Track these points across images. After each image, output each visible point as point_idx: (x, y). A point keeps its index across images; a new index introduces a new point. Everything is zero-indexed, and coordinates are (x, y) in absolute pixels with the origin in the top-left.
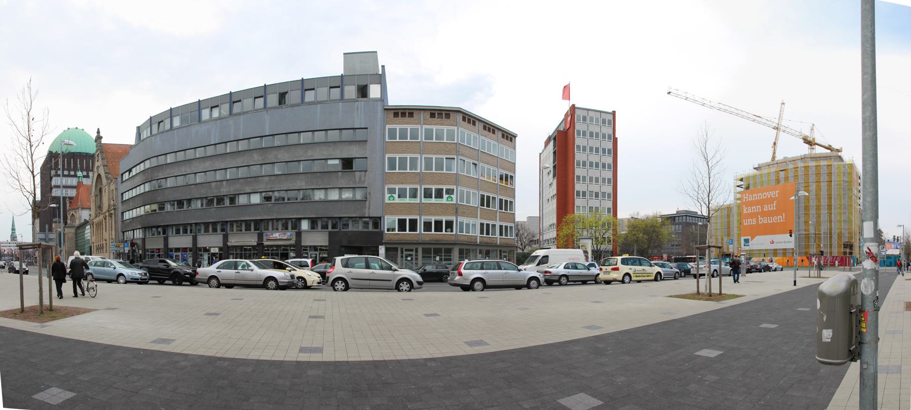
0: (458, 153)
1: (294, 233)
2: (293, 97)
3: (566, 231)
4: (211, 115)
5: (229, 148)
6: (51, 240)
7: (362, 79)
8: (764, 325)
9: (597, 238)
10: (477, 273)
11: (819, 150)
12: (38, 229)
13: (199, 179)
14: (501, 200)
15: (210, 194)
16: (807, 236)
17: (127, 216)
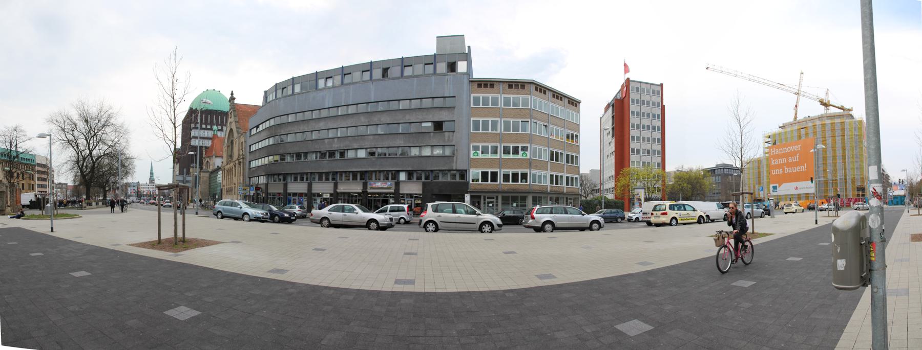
0: (531, 117)
1: (393, 182)
2: (395, 72)
3: (623, 182)
4: (326, 84)
5: (340, 112)
6: (188, 182)
7: (451, 57)
8: (790, 259)
9: (648, 188)
10: (547, 217)
11: (833, 110)
12: (177, 172)
13: (315, 136)
14: (568, 155)
15: (323, 149)
16: (826, 182)
17: (254, 164)
